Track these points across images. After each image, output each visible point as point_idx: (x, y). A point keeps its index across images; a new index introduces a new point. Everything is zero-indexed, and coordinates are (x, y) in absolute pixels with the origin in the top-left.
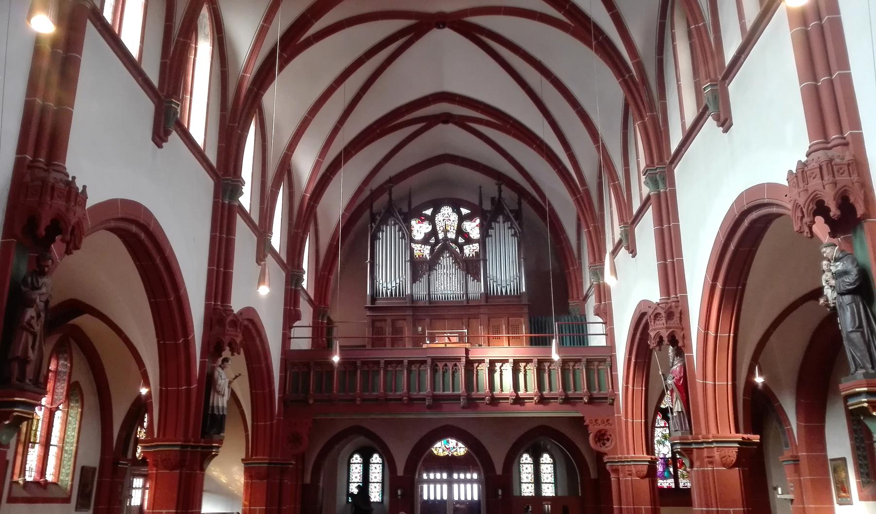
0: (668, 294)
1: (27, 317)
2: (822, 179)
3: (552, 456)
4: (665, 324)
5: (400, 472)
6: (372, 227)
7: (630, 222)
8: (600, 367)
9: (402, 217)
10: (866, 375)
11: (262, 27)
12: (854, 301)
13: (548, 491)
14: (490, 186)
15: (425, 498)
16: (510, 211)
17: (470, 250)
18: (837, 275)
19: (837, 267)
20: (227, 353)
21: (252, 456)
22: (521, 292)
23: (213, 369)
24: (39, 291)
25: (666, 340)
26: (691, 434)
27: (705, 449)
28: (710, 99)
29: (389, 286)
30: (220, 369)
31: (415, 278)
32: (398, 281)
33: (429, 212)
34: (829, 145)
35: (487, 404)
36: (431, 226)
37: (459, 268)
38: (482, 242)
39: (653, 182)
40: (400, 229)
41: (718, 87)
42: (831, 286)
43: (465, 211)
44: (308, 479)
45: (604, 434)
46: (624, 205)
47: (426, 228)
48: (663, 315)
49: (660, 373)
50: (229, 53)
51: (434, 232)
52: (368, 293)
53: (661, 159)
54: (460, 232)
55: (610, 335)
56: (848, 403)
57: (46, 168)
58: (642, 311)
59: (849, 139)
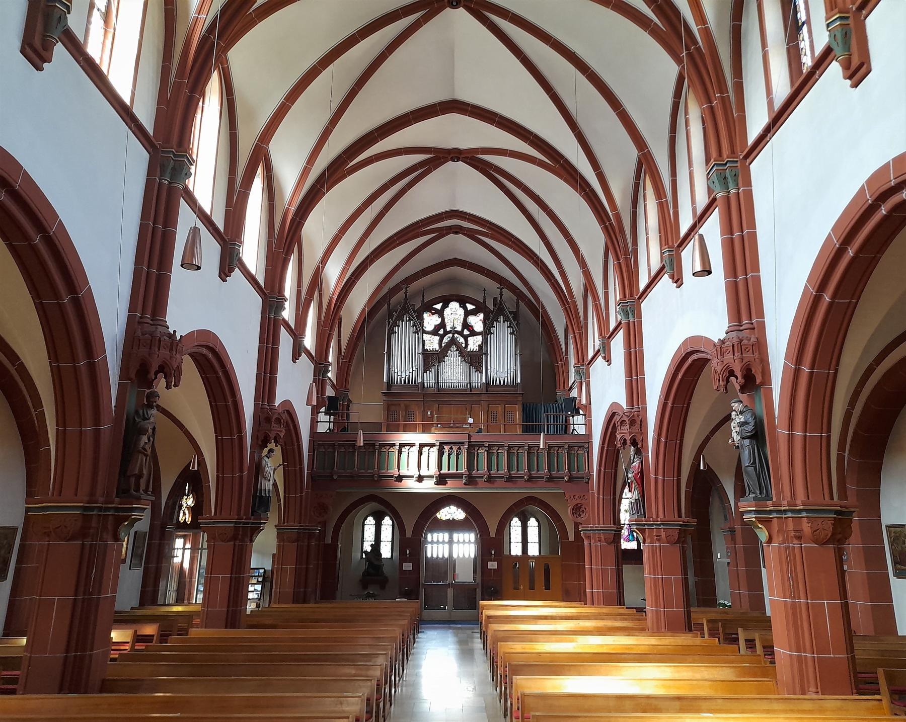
0: (739, 320)
1: (142, 444)
2: (734, 355)
3: (537, 520)
4: (628, 429)
5: (409, 534)
6: (389, 322)
7: (607, 338)
8: (579, 452)
9: (416, 314)
10: (755, 499)
11: (305, 168)
12: (751, 444)
13: (533, 550)
14: (493, 286)
15: (429, 555)
16: (509, 312)
17: (474, 343)
18: (741, 424)
19: (740, 419)
20: (271, 445)
21: (284, 523)
22: (517, 382)
23: (261, 459)
24: (148, 421)
25: (628, 442)
26: (645, 517)
27: (655, 529)
28: (668, 261)
29: (403, 375)
30: (266, 458)
31: (426, 368)
32: (411, 371)
33: (438, 306)
34: (741, 328)
35: (485, 481)
36: (440, 319)
37: (464, 360)
38: (486, 333)
39: (626, 313)
40: (414, 325)
41: (674, 253)
42: (736, 432)
43: (470, 307)
44: (329, 540)
45: (580, 507)
46: (603, 322)
47: (436, 320)
48: (627, 422)
49: (624, 467)
50: (275, 184)
51: (443, 325)
52: (385, 380)
53: (632, 295)
54: (466, 325)
55: (588, 425)
56: (744, 517)
57: (151, 322)
58: (613, 411)
59: (755, 325)
